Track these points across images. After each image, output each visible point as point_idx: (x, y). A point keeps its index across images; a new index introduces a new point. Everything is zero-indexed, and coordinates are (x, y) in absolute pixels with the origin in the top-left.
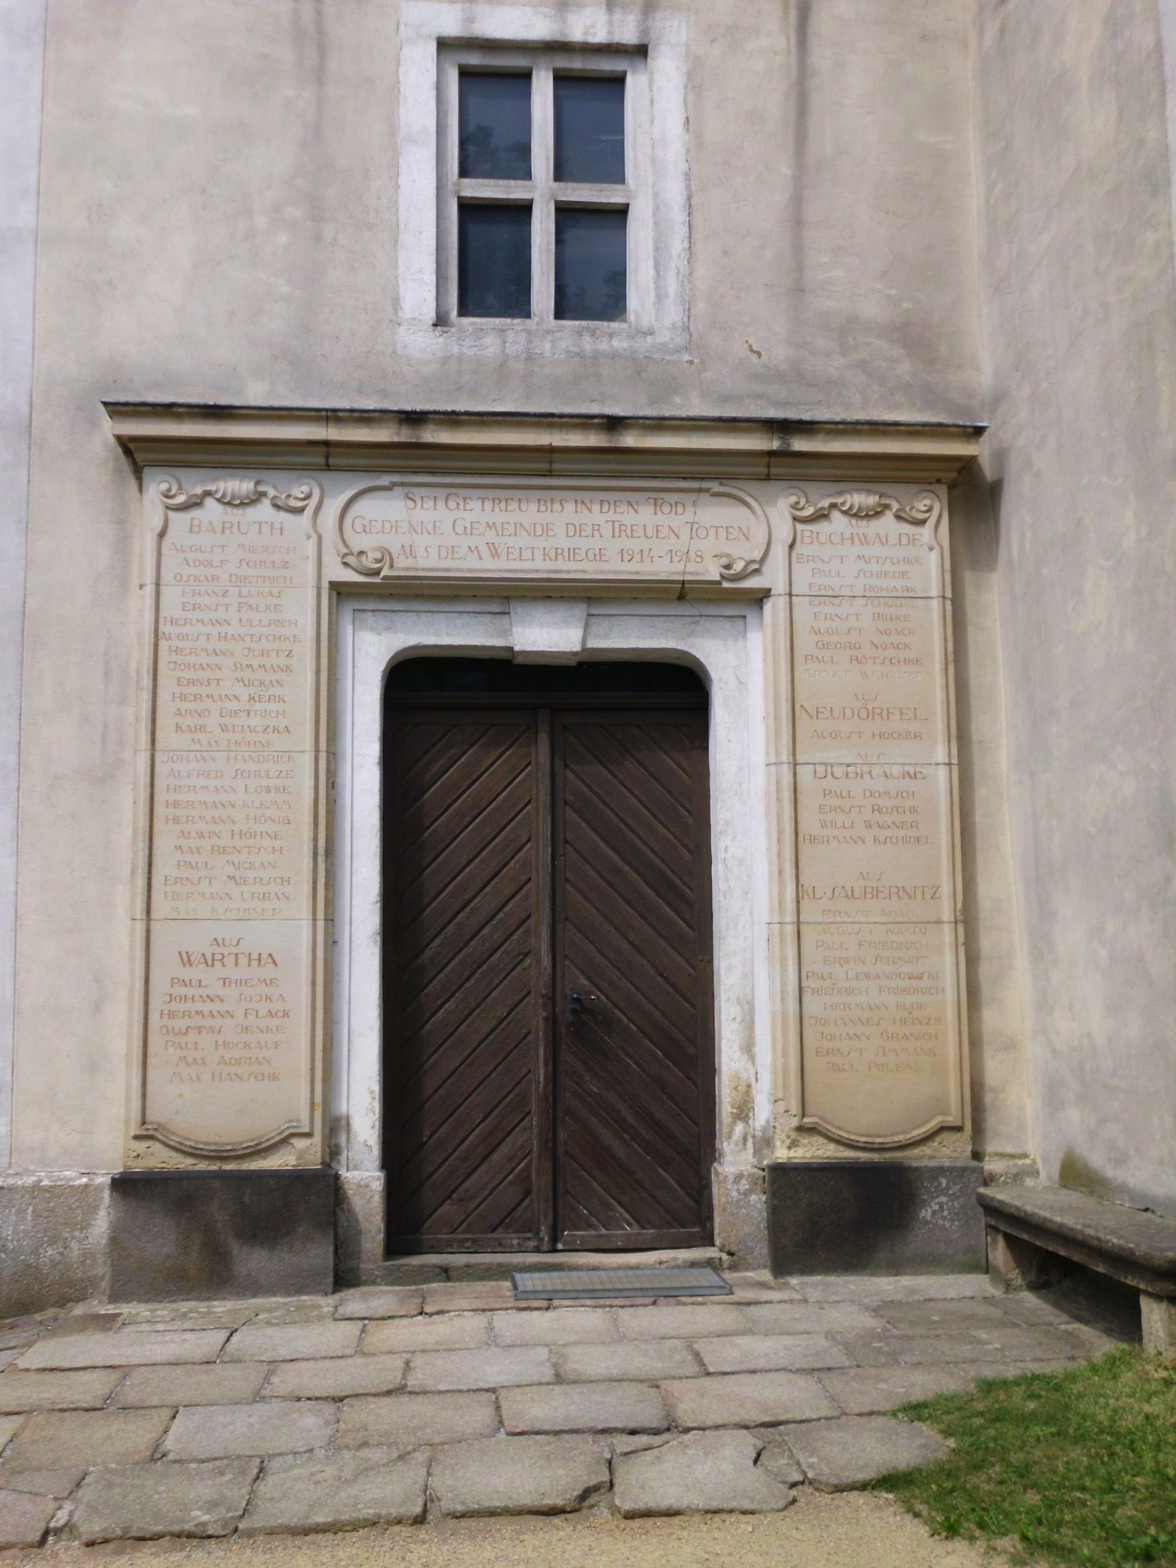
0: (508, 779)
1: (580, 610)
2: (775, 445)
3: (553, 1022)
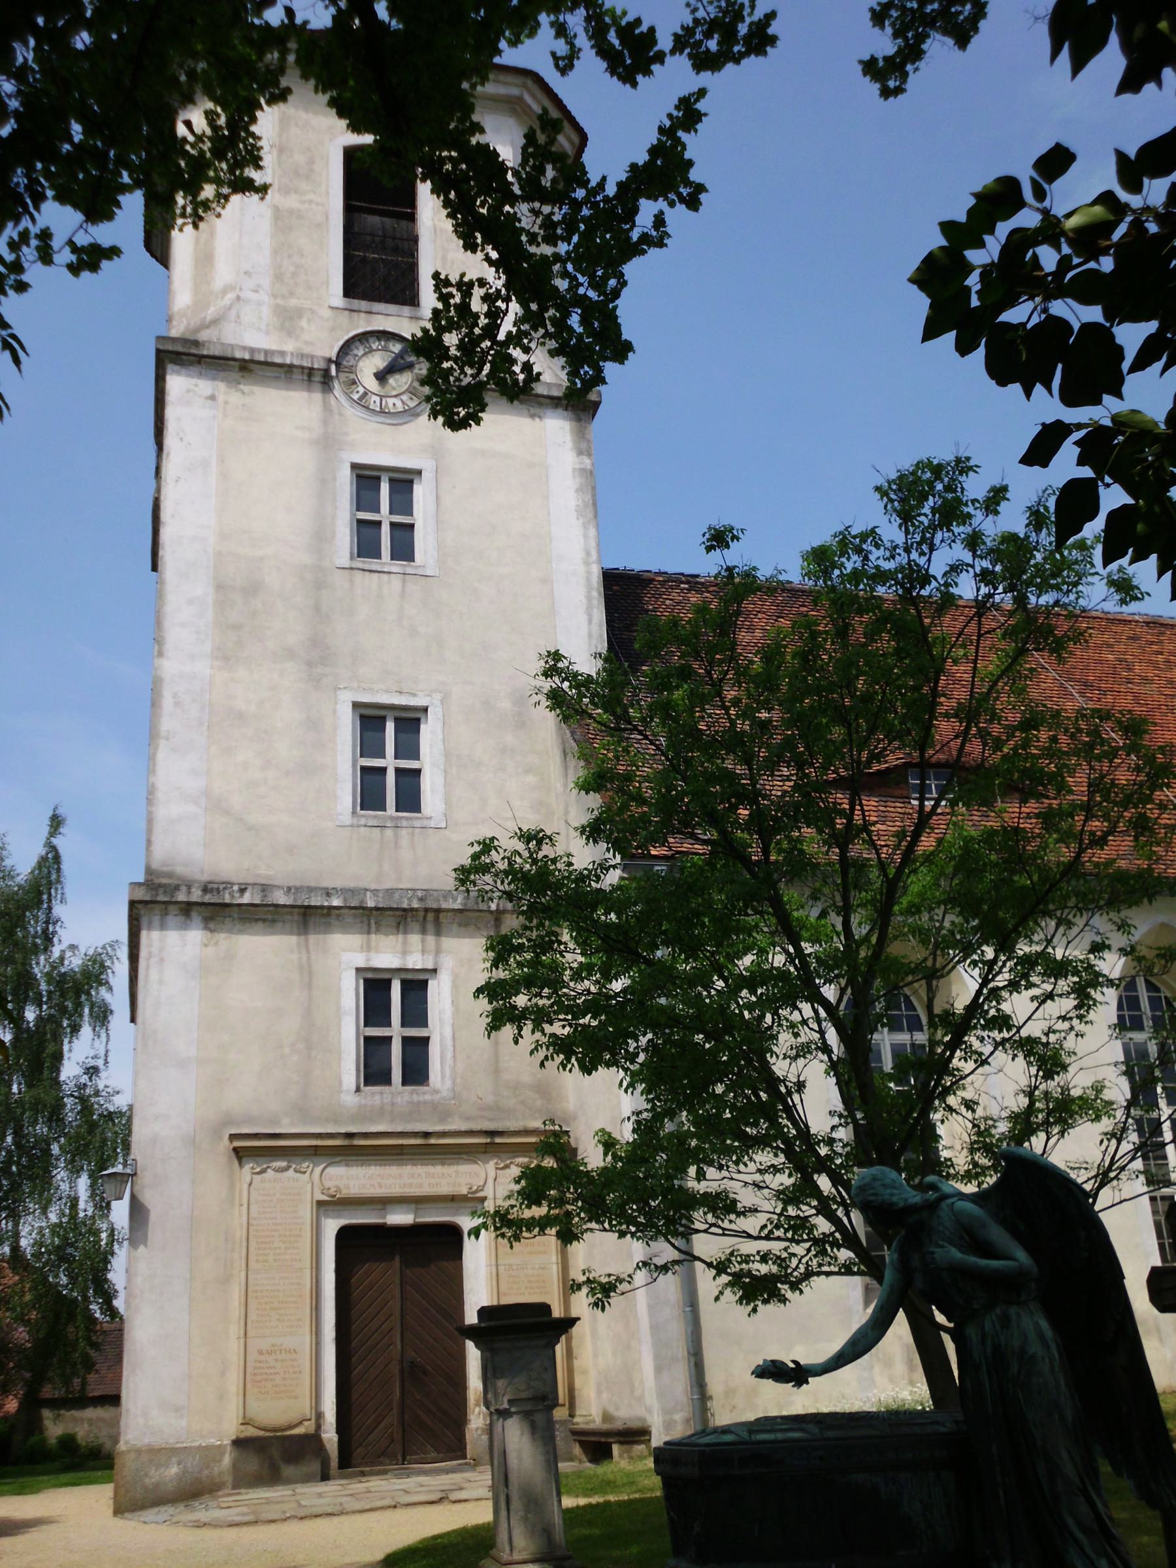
0: (384, 1276)
1: (413, 1206)
2: (488, 1140)
3: (402, 1371)
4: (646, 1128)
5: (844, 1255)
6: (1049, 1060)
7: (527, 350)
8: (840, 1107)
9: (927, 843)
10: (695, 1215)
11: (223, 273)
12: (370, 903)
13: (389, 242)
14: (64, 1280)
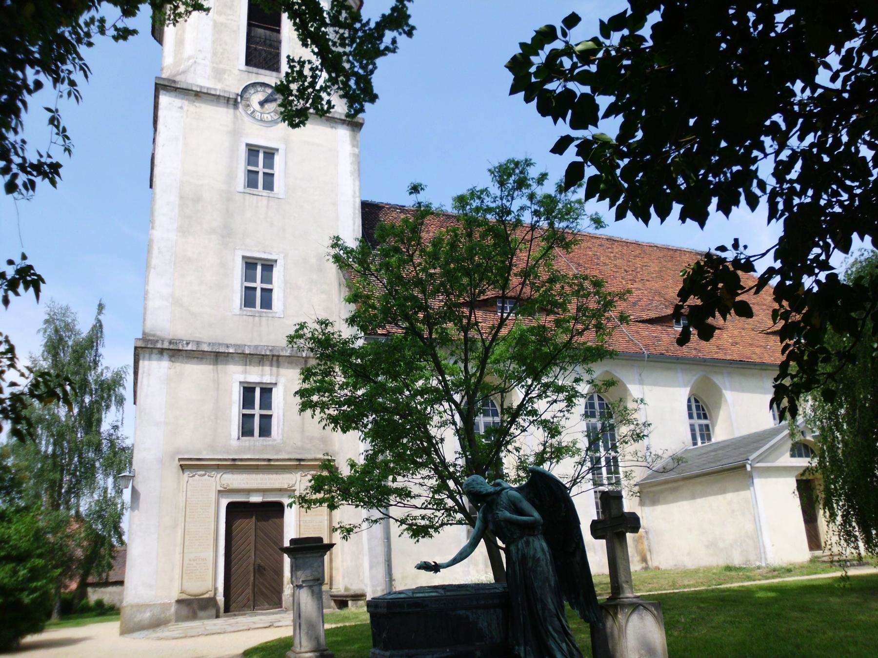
0: (247, 525)
3: (254, 569)
4: (371, 459)
5: (459, 516)
6: (553, 430)
7: (329, 94)
8: (460, 450)
9: (504, 332)
10: (391, 497)
11: (189, 49)
12: (247, 352)
13: (268, 42)
14: (100, 527)
